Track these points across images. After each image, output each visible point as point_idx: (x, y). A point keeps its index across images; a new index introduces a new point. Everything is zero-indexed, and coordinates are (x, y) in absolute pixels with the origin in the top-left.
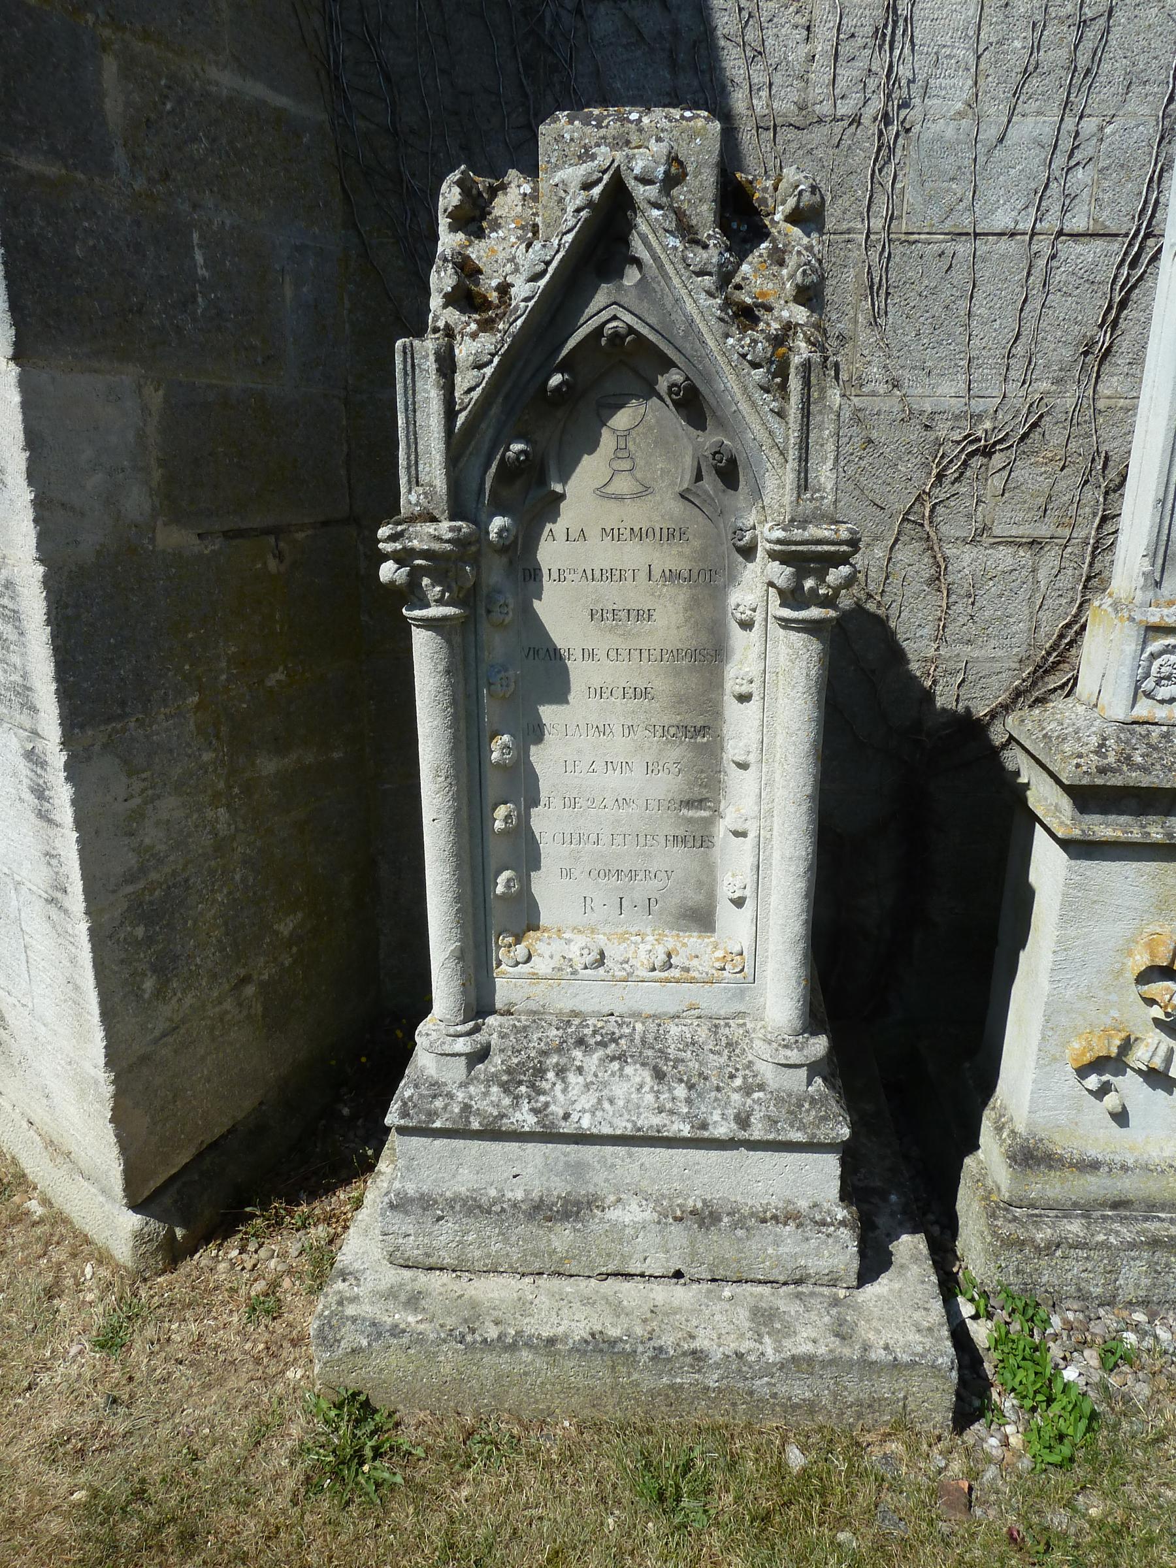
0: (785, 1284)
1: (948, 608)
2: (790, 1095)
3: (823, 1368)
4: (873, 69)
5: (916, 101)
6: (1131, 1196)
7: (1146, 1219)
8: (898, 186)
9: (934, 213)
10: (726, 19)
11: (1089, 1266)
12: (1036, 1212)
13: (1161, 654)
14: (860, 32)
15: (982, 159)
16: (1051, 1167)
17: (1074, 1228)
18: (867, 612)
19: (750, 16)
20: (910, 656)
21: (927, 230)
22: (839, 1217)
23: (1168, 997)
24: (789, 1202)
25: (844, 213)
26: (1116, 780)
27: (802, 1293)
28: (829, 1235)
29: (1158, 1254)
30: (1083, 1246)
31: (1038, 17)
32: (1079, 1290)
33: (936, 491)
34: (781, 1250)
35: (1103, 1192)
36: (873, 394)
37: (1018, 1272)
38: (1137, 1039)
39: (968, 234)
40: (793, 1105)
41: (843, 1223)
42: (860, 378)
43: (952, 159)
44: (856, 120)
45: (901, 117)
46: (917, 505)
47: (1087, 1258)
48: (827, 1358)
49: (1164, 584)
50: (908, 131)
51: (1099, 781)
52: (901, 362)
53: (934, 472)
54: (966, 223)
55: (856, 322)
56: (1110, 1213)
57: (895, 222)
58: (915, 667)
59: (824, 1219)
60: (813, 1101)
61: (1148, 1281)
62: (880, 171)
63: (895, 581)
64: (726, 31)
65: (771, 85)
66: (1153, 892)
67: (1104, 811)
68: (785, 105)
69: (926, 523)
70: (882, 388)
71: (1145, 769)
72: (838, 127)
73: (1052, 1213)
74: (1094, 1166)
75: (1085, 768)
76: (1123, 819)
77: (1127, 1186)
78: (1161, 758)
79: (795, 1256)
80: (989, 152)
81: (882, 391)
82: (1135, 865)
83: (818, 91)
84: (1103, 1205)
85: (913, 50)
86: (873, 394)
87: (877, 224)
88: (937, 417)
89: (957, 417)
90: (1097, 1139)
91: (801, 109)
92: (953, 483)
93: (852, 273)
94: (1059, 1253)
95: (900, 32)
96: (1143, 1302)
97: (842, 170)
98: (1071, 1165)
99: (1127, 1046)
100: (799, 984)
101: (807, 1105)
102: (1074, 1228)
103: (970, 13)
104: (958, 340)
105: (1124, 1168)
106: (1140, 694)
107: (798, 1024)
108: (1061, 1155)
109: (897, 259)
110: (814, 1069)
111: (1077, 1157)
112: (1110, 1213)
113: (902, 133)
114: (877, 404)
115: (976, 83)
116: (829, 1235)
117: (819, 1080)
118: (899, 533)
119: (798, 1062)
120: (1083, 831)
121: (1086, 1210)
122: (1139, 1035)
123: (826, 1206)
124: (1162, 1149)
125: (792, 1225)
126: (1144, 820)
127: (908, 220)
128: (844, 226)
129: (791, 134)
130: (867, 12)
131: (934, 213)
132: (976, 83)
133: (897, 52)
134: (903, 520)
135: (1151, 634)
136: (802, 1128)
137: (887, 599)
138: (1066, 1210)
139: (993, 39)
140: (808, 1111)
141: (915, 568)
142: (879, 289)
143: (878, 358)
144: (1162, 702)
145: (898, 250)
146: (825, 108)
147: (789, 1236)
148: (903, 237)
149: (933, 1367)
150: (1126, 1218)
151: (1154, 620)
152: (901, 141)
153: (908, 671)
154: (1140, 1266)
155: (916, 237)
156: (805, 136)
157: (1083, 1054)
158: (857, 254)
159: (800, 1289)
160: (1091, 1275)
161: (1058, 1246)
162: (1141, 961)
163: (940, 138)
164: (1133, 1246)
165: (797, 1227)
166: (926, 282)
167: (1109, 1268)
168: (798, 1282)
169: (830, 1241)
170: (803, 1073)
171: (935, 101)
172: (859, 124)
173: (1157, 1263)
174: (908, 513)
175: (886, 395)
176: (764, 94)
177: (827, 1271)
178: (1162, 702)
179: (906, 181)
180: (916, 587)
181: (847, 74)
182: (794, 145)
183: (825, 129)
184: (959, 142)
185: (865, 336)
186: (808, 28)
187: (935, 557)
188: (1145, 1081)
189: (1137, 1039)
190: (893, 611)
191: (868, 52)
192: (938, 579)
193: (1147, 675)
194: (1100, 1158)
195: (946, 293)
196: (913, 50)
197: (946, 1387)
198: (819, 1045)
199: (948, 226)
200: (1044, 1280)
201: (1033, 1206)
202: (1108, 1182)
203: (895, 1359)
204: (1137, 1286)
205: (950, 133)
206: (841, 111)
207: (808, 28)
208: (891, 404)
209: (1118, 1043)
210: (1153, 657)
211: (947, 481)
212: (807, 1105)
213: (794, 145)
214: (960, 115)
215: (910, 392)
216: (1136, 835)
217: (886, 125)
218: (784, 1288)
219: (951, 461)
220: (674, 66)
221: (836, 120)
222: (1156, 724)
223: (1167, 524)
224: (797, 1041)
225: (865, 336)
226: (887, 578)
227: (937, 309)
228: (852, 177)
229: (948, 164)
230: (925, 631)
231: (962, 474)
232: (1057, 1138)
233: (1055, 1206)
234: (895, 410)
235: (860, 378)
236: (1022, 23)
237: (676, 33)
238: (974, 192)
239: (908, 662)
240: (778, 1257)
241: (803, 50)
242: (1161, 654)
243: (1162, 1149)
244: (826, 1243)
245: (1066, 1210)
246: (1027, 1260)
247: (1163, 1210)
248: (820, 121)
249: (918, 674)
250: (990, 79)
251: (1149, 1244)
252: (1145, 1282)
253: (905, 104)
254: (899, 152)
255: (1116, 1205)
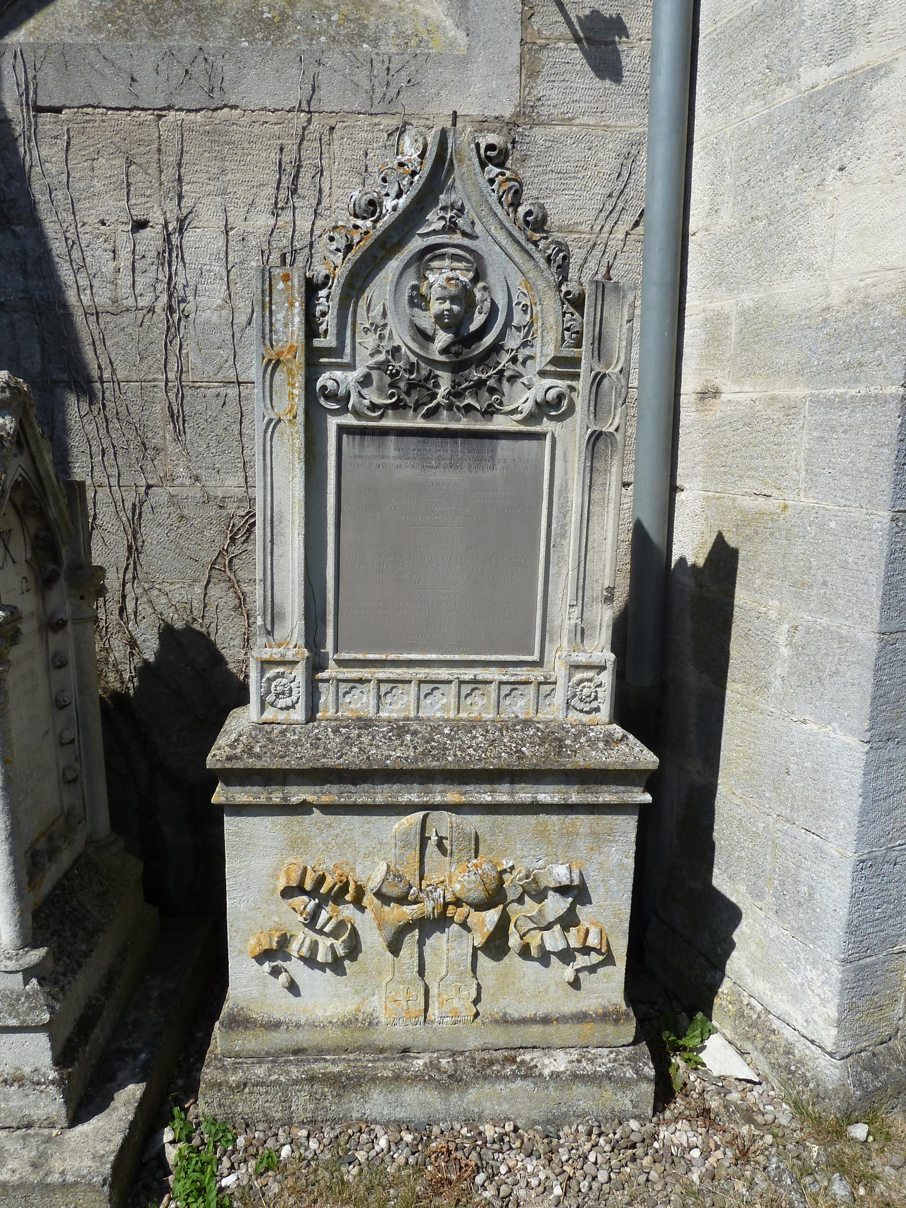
0: (18, 1128)
1: (249, 626)
2: (12, 993)
3: (14, 1191)
4: (160, 278)
5: (191, 298)
6: (305, 1045)
7: (316, 1060)
8: (184, 352)
9: (210, 369)
10: (57, 245)
11: (269, 1098)
12: (240, 1060)
13: (275, 678)
14: (148, 255)
15: (238, 335)
16: (246, 1028)
17: (260, 1071)
18: (194, 630)
19: (74, 243)
20: (228, 659)
21: (206, 380)
22: (50, 1078)
23: (302, 907)
24: (18, 1069)
25: (149, 368)
26: (239, 765)
27: (28, 1135)
28: (41, 1092)
29: (315, 1086)
30: (262, 1084)
31: (265, 247)
32: (266, 1115)
33: (231, 549)
34: (11, 1104)
35: (285, 1043)
36: (182, 485)
37: (220, 1105)
38: (292, 936)
39: (233, 382)
40: (13, 1001)
41: (53, 1082)
42: (171, 475)
43: (218, 335)
44: (151, 310)
45: (181, 309)
46: (220, 558)
47: (266, 1092)
48: (17, 1183)
49: (276, 632)
50: (187, 317)
51: (228, 766)
52: (199, 464)
53: (229, 536)
54: (232, 375)
55: (165, 439)
56: (292, 1058)
57: (184, 375)
58: (231, 666)
59: (40, 1080)
60: (28, 996)
61: (312, 1106)
62: (171, 342)
63: (211, 609)
64: (58, 252)
65: (91, 287)
66: (286, 836)
67: (242, 784)
68: (103, 298)
69: (227, 569)
70: (187, 482)
71: (259, 757)
72: (140, 314)
73: (250, 1061)
74: (276, 1025)
75: (218, 758)
76: (255, 789)
77: (301, 1038)
78: (273, 748)
79: (21, 1108)
80: (243, 330)
81: (188, 484)
82: (270, 818)
83: (124, 290)
84: (287, 1052)
85: (185, 266)
86: (182, 485)
87: (172, 375)
88: (227, 500)
89: (240, 500)
90: (280, 1006)
91: (114, 302)
92: (243, 543)
93: (159, 407)
94: (247, 1090)
95: (174, 255)
96: (311, 1121)
97: (146, 341)
98: (262, 1026)
99: (284, 941)
100: (15, 914)
101: (23, 999)
102: (260, 1071)
103: (220, 244)
104: (235, 450)
105: (298, 1026)
106: (267, 705)
107: (19, 943)
108: (256, 1019)
109: (189, 398)
110: (28, 973)
111: (266, 1019)
112: (292, 1058)
113: (183, 319)
114: (185, 492)
115: (229, 288)
116: (41, 1092)
117: (34, 981)
118: (210, 577)
119: (14, 969)
120: (227, 798)
121: (274, 1057)
122: (295, 933)
123: (43, 1070)
124: (325, 1010)
125: (16, 1085)
126: (270, 789)
127: (193, 373)
128: (151, 377)
129: (109, 318)
130: (152, 242)
131: (210, 369)
132: (229, 288)
133: (174, 268)
134: (212, 568)
135: (266, 666)
136: (17, 1016)
137: (207, 621)
138: (260, 1058)
139: (237, 261)
140: (23, 1003)
141: (224, 600)
142: (178, 417)
143: (183, 461)
144: (281, 709)
145: (188, 392)
146: (131, 302)
147: (14, 1094)
148: (191, 384)
149: (89, 1184)
150: (302, 1061)
151: (266, 657)
152: (183, 323)
153: (227, 670)
154: (304, 1097)
155: (200, 384)
156: (118, 319)
157: (255, 948)
158: (161, 395)
159: (29, 1131)
160: (272, 1105)
161: (245, 1085)
162: (282, 884)
163: (209, 322)
164: (296, 1082)
165: (19, 1087)
166: (210, 413)
167: (283, 1099)
168: (29, 1126)
169: (43, 1095)
170: (20, 977)
171: (203, 298)
172: (154, 312)
173: (316, 1093)
174: (214, 563)
175: (190, 486)
176: (88, 292)
177: (44, 1117)
178: (281, 709)
179: (189, 348)
180: (226, 612)
181: (141, 281)
182: (112, 325)
183: (132, 315)
184: (221, 325)
185: (172, 447)
186: (114, 252)
187: (236, 593)
188: (305, 964)
189: (292, 936)
190: (212, 629)
191: (155, 267)
192: (240, 606)
193: (268, 692)
194: (282, 1019)
195: (224, 420)
196: (185, 266)
197: (102, 1198)
198: (36, 955)
199: (220, 377)
200: (240, 1110)
201: (238, 1056)
202: (287, 1036)
203: (64, 1181)
204: (305, 1110)
205: (215, 318)
206: (140, 304)
207: (114, 252)
208: (195, 492)
209: (276, 939)
210: (270, 680)
211: (239, 542)
212: (23, 999)
213: (112, 325)
214: (221, 307)
215: (207, 484)
216: (262, 800)
217: (171, 313)
218: (18, 1132)
219: (239, 529)
220: (25, 274)
221: (137, 309)
222: (279, 723)
223: (269, 594)
224: (17, 954)
225: (172, 447)
226: (205, 607)
227: (219, 431)
228: (153, 346)
229: (216, 338)
230: (236, 642)
231: (248, 538)
232: (252, 1006)
233: (254, 1055)
234: (198, 496)
235: (171, 475)
236: (255, 251)
237: (24, 252)
238: (235, 356)
239: (227, 663)
240: (9, 1109)
241: (112, 265)
242: (275, 678)
243: (325, 1010)
244: (40, 1097)
245: (260, 1058)
246: (225, 1097)
247: (329, 1054)
248: (127, 310)
249: (235, 671)
250: (238, 285)
251: (307, 1080)
252: (311, 1107)
253: (183, 300)
254: (182, 330)
255: (296, 1052)
